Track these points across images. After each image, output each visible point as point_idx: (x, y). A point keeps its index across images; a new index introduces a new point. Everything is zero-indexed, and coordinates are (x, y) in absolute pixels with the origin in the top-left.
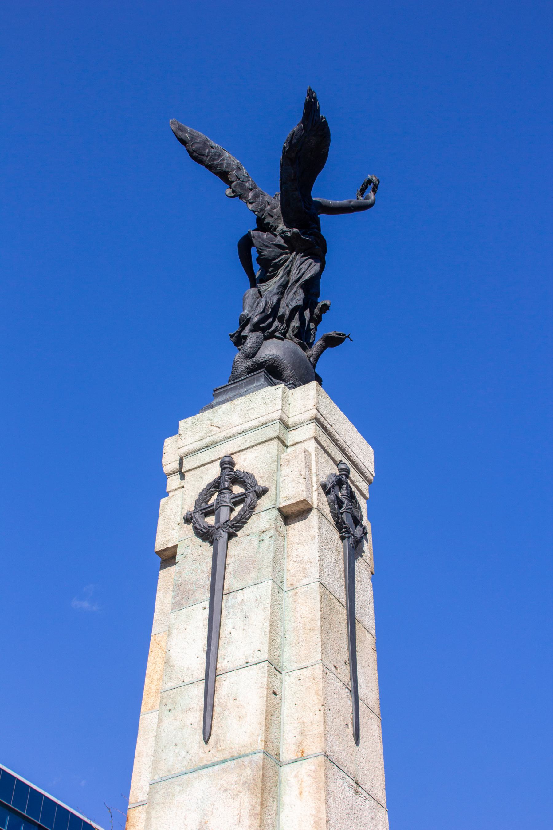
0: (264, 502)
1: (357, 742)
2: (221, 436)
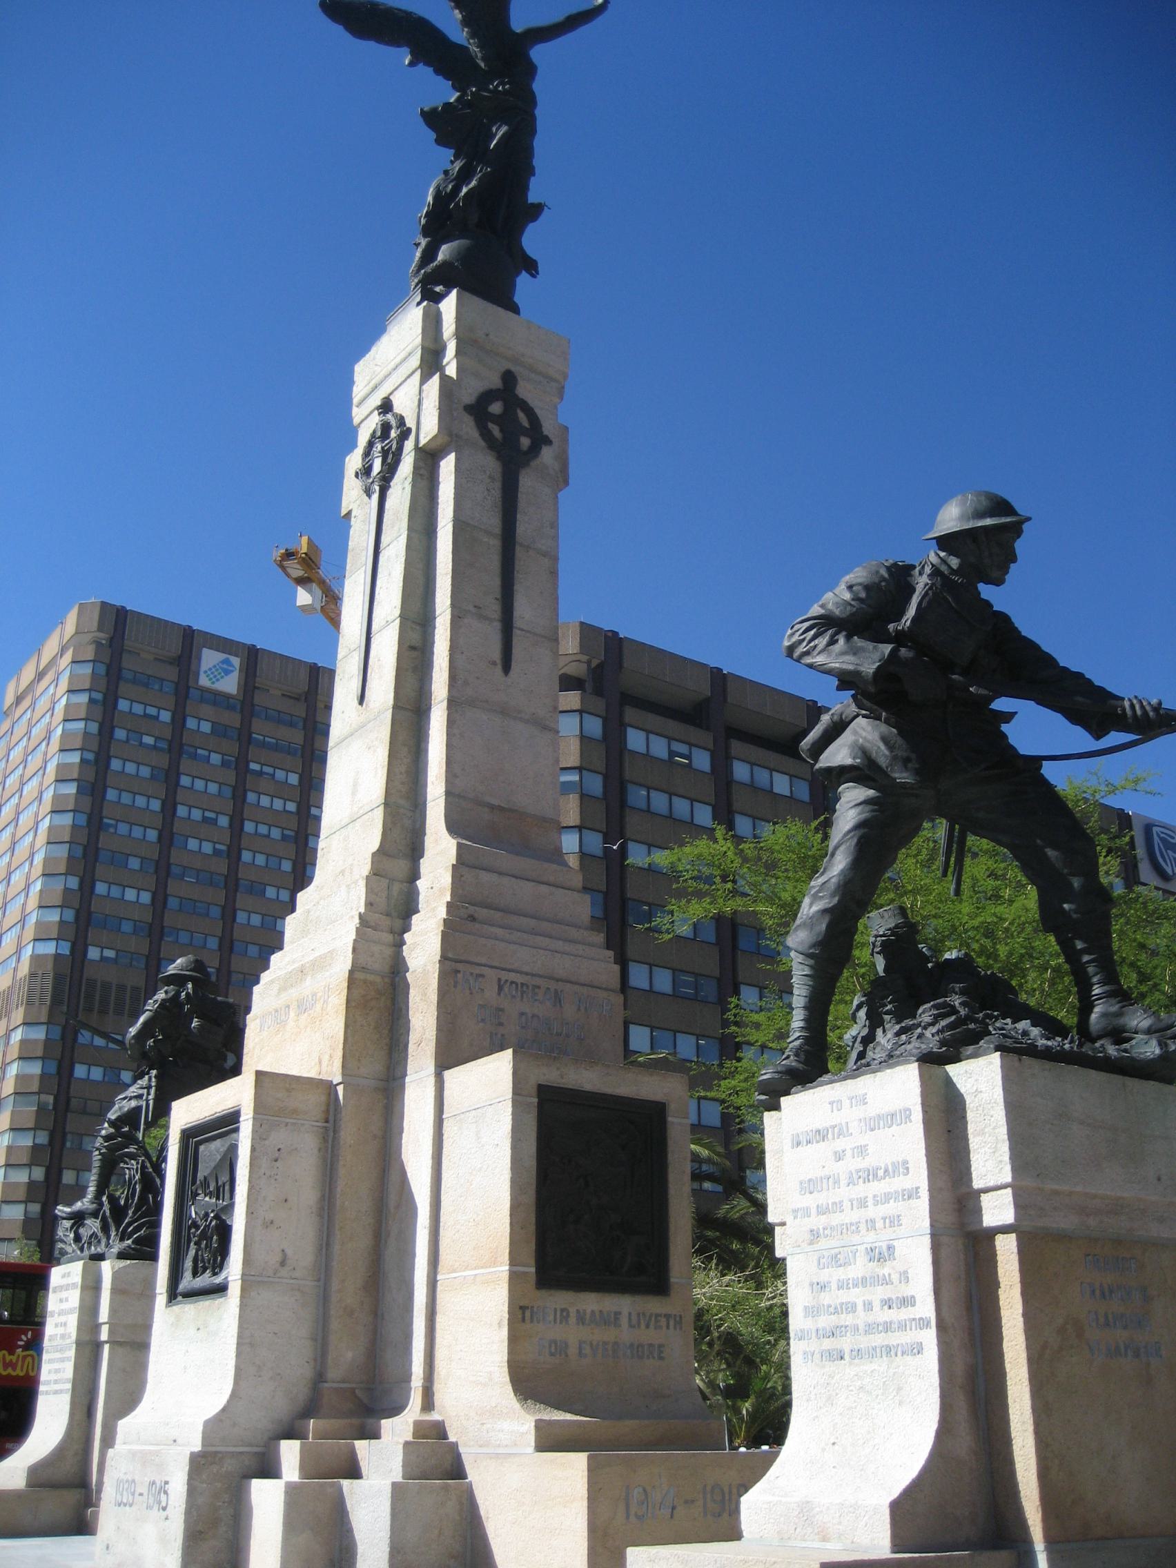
0: (409, 445)
1: (507, 666)
2: (381, 376)
